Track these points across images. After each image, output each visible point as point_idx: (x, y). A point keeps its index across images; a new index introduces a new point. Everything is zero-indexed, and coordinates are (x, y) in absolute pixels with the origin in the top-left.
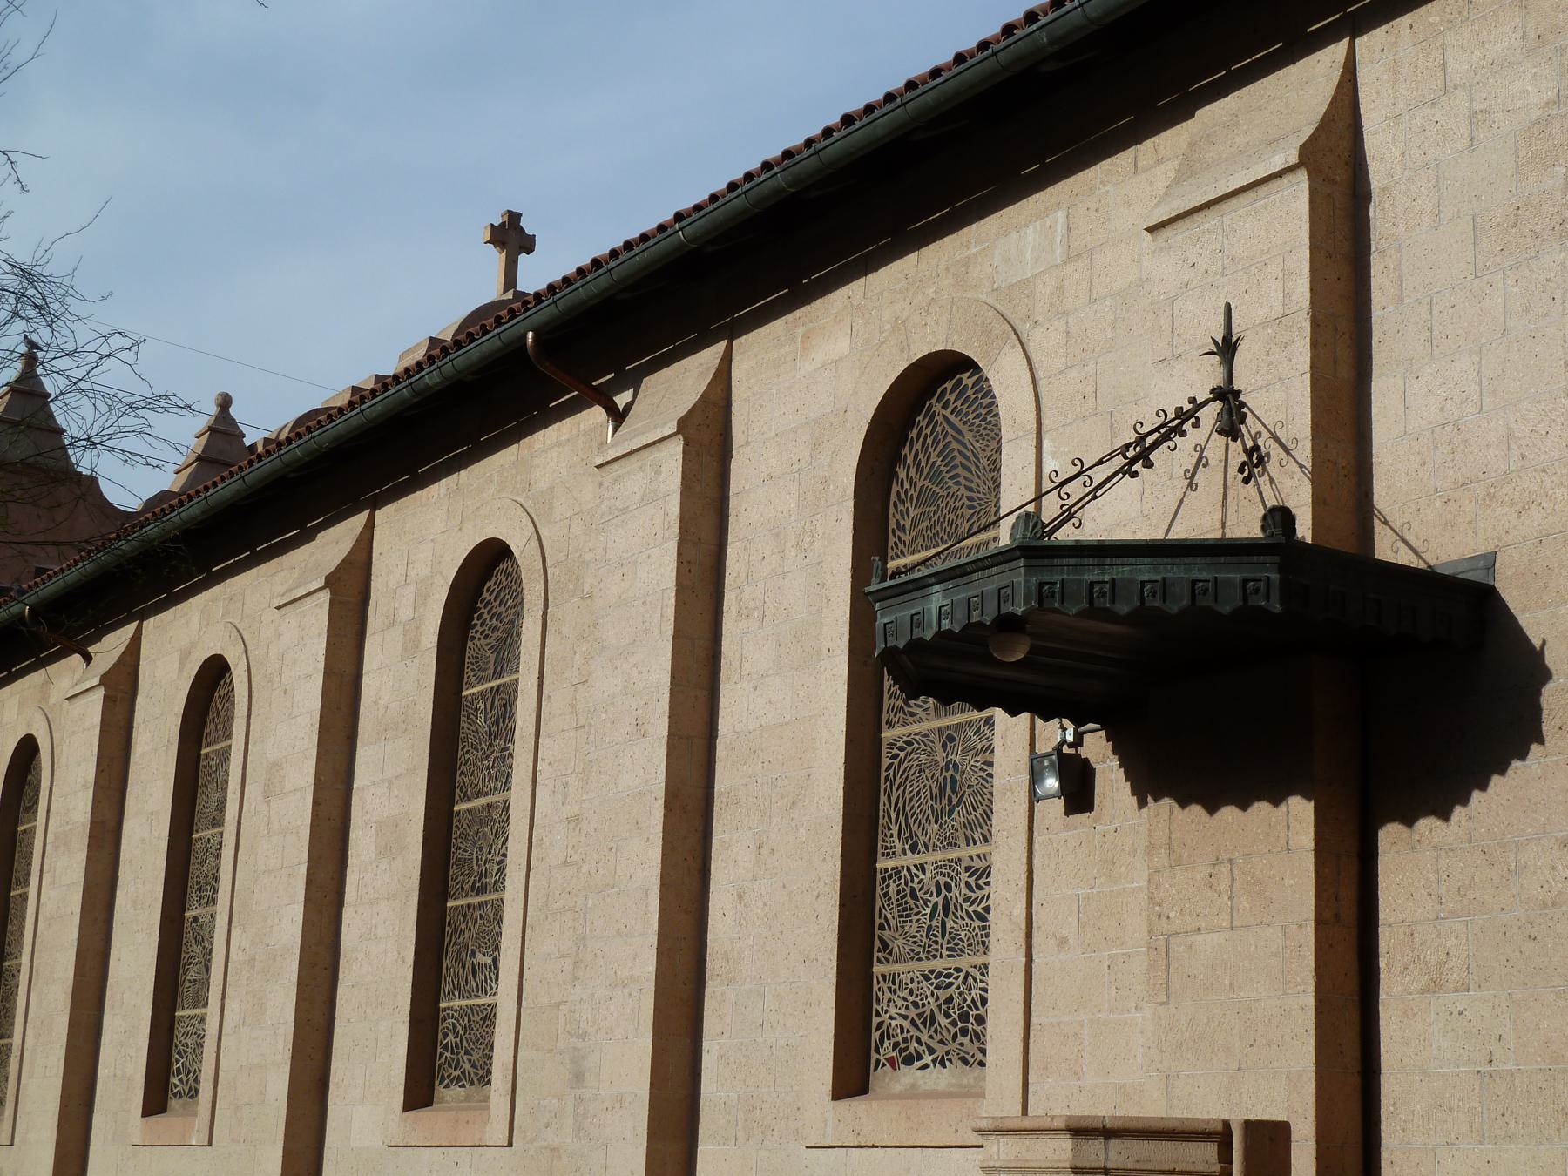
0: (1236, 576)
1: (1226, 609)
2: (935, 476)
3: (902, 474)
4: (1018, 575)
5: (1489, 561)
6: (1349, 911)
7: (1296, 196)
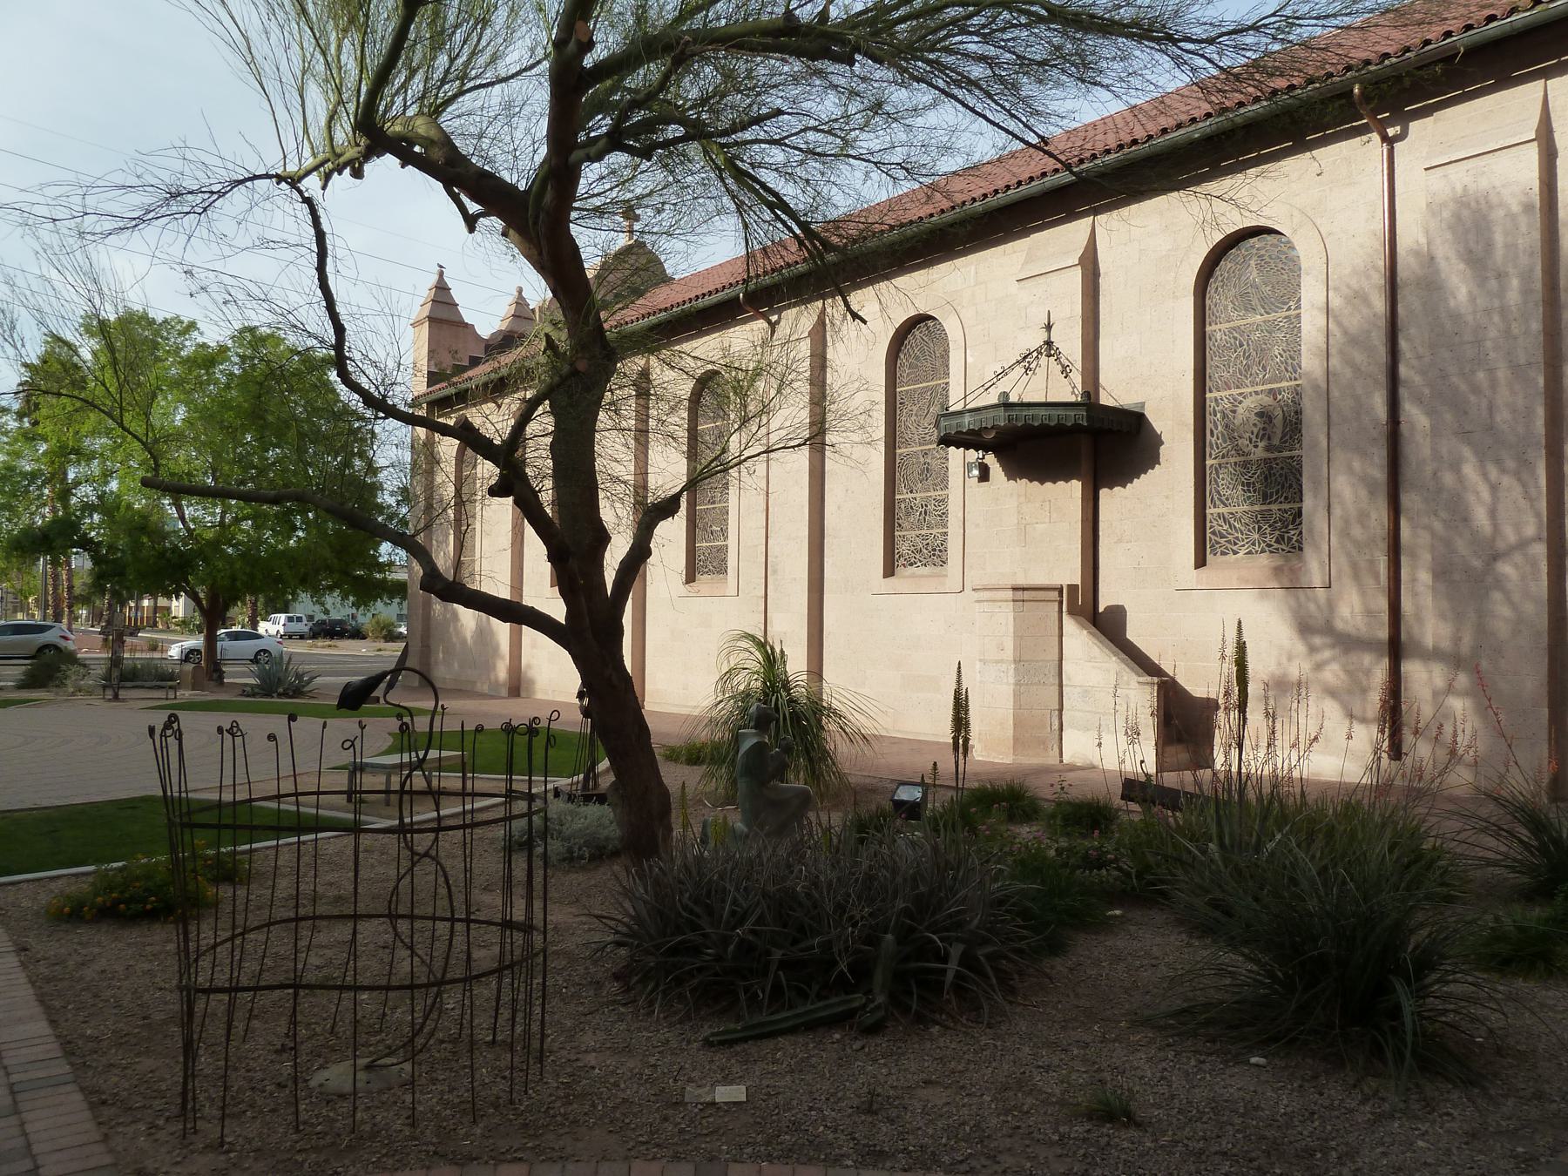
0: (1073, 414)
1: (1069, 424)
2: (917, 358)
3: (902, 356)
4: (1001, 412)
5: (1143, 404)
6: (1090, 517)
7: (1077, 274)
